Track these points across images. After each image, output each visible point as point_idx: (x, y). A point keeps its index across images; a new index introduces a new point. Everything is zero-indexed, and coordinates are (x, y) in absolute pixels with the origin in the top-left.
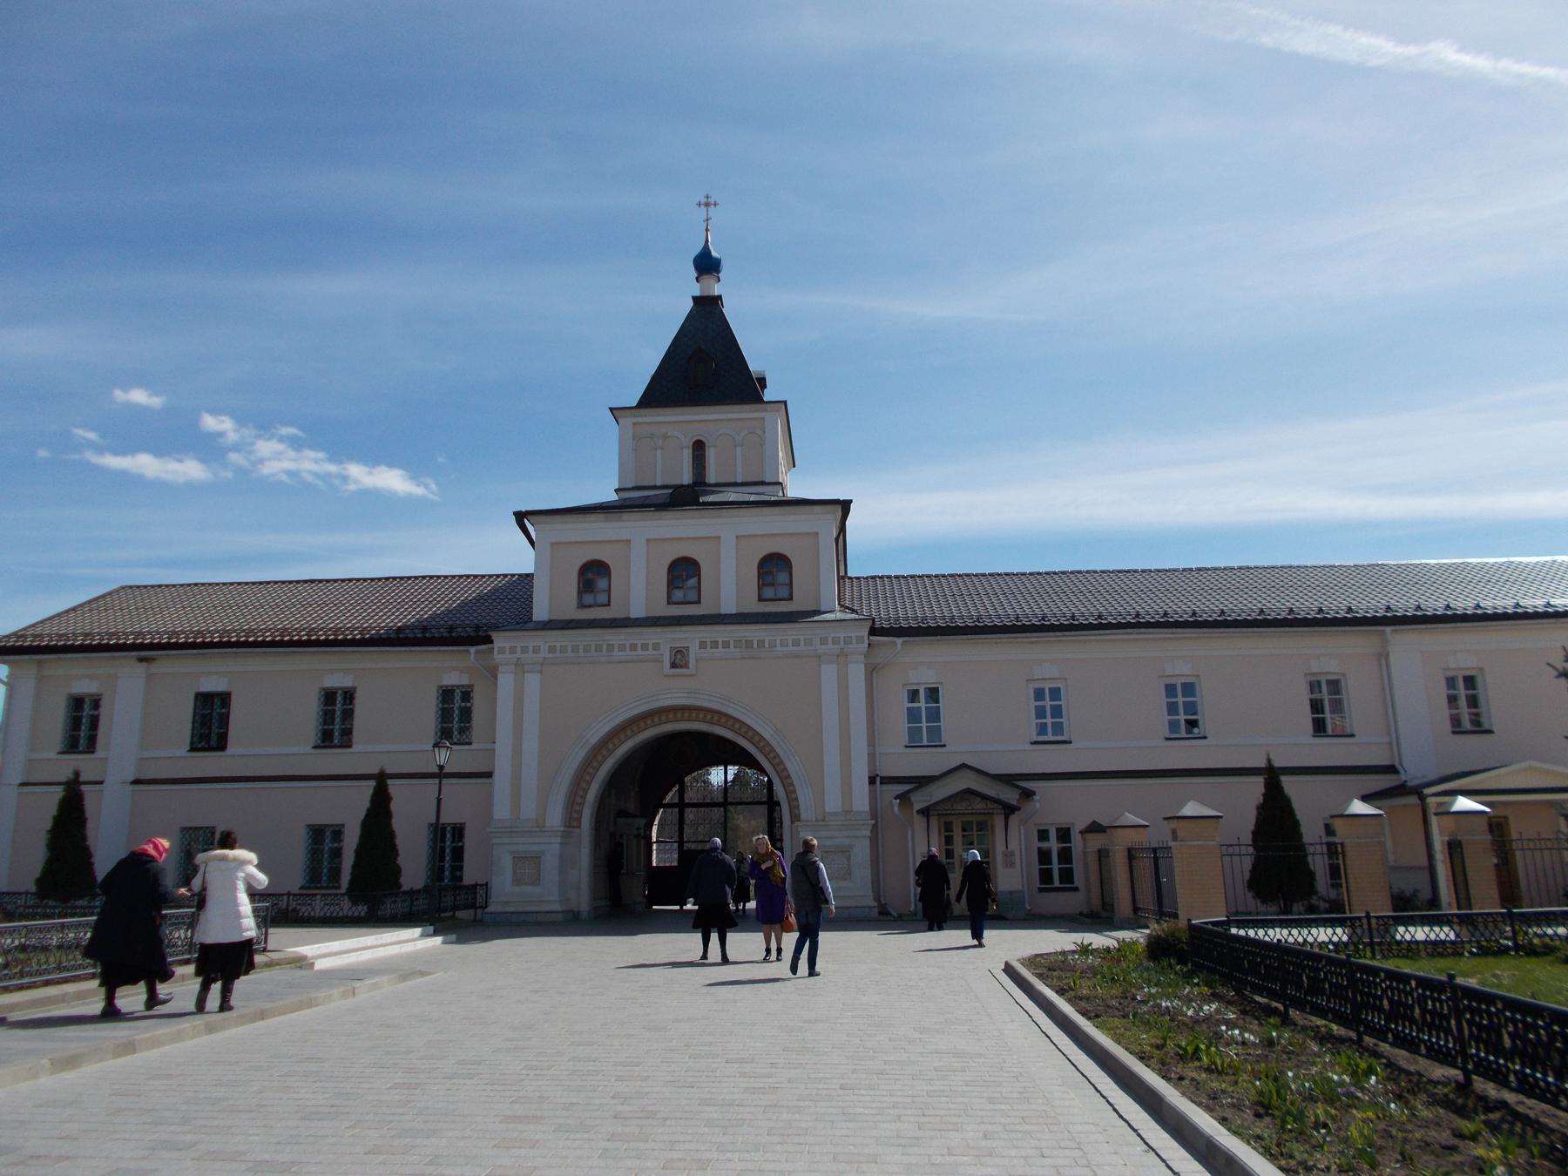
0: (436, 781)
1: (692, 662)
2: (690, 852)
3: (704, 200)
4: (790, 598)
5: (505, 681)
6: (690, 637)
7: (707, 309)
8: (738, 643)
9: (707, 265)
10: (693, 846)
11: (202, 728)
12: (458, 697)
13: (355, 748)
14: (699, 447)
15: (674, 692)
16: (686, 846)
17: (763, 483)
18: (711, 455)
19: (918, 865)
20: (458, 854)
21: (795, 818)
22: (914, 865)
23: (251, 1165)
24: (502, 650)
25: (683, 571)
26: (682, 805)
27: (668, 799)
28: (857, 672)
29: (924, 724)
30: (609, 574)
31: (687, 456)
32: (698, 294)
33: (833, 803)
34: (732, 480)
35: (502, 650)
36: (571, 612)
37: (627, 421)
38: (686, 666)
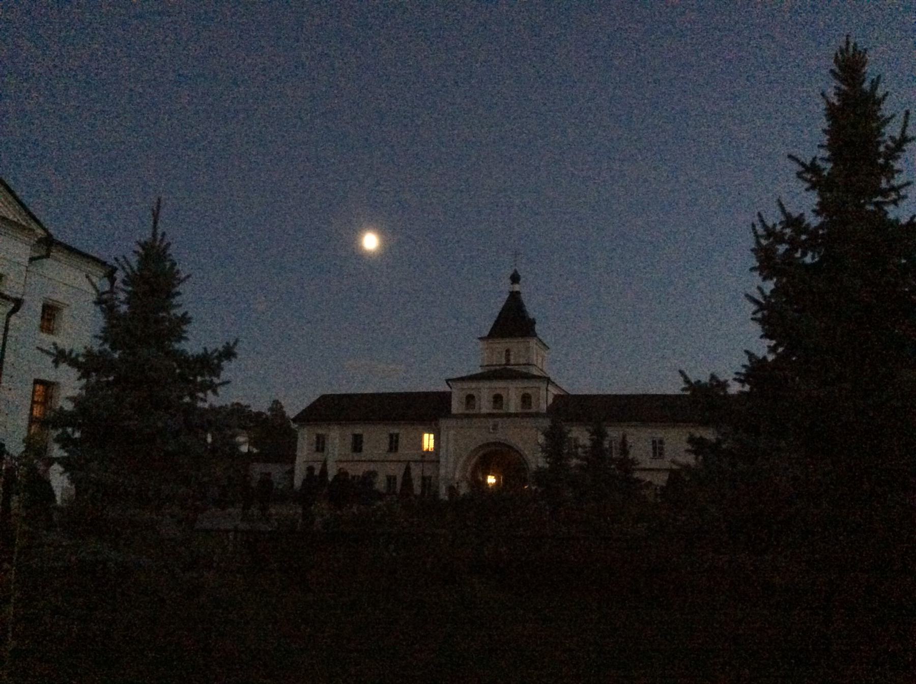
14: (508, 351)
25: (498, 399)
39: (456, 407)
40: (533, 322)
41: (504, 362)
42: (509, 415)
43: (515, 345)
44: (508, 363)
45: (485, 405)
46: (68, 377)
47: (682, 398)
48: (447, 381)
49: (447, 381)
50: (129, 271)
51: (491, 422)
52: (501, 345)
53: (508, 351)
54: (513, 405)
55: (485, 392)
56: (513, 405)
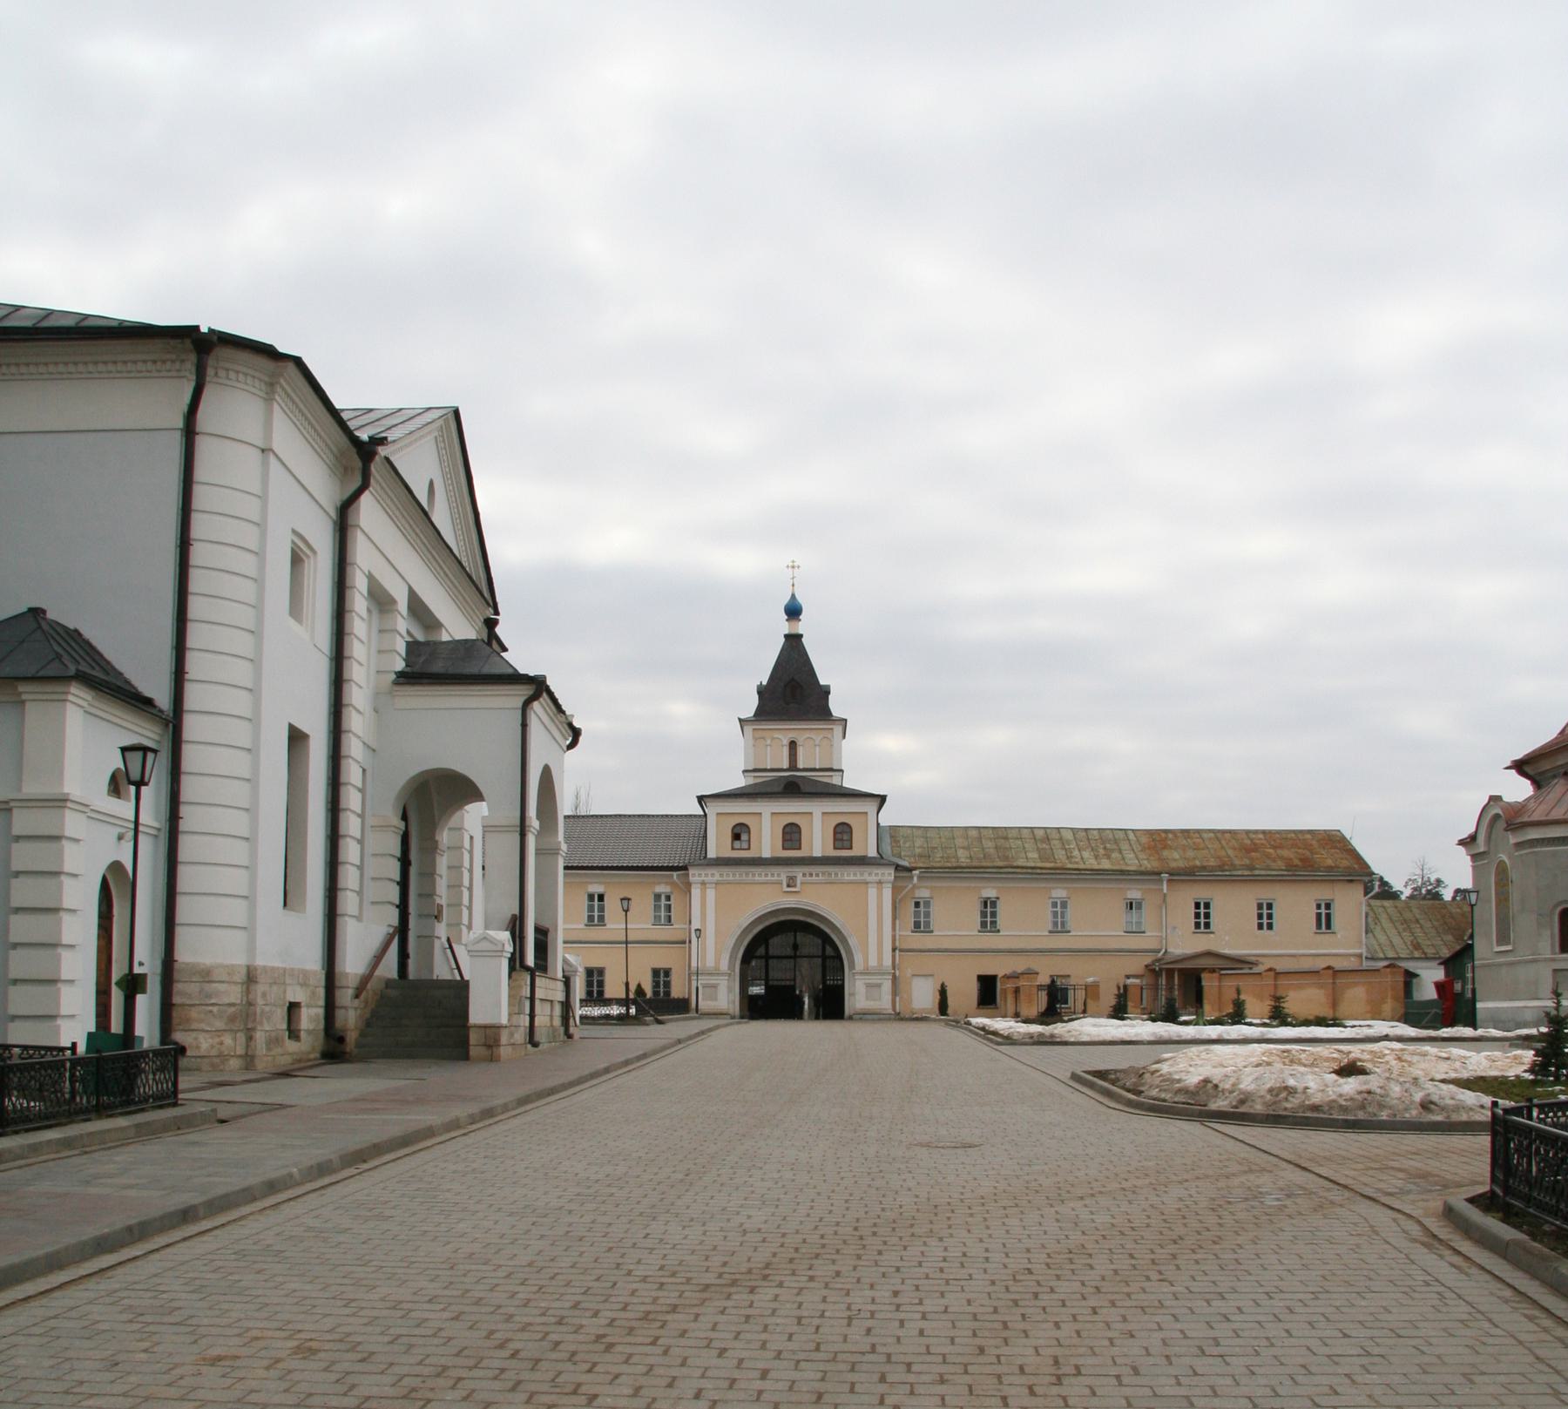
0: (792, 960)
1: (799, 882)
2: (773, 986)
3: (791, 564)
4: (851, 848)
5: (696, 892)
6: (798, 872)
7: (793, 642)
8: (823, 874)
9: (793, 612)
10: (775, 983)
11: (1531, 1071)
12: (663, 897)
13: (608, 926)
14: (793, 745)
15: (789, 902)
16: (771, 983)
17: (831, 770)
18: (800, 751)
19: (372, 481)
20: (601, 984)
21: (852, 966)
22: (374, 477)
23: (246, 1293)
24: (694, 875)
25: (792, 834)
26: (767, 957)
27: (758, 953)
28: (887, 893)
29: (922, 920)
30: (749, 832)
31: (786, 751)
32: (787, 632)
33: (873, 962)
34: (812, 767)
35: (694, 875)
36: (728, 853)
37: (749, 729)
38: (795, 886)
39: (717, 845)
40: (826, 692)
41: (786, 765)
42: (758, 862)
43: (808, 735)
44: (793, 766)
45: (767, 842)
46: (262, 1065)
47: (788, 837)
48: (701, 799)
49: (701, 799)
50: (116, 1026)
51: (782, 874)
52: (781, 734)
53: (793, 745)
54: (818, 842)
55: (767, 820)
56: (818, 842)
